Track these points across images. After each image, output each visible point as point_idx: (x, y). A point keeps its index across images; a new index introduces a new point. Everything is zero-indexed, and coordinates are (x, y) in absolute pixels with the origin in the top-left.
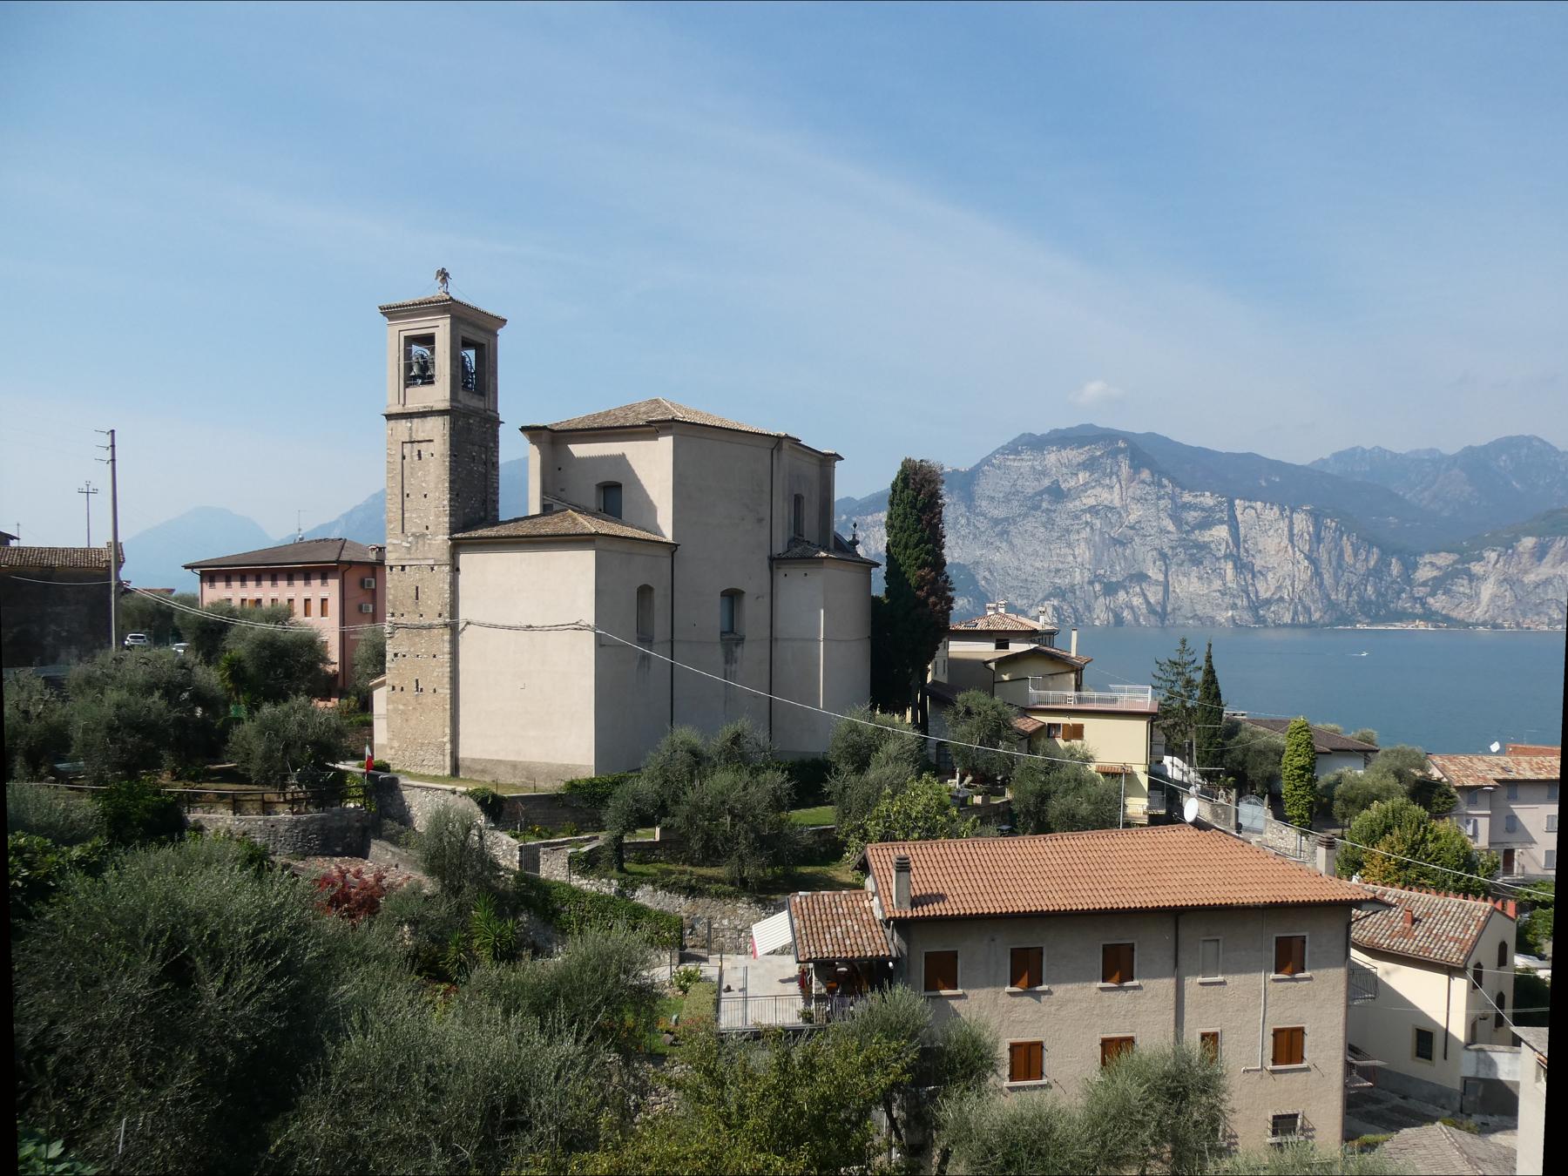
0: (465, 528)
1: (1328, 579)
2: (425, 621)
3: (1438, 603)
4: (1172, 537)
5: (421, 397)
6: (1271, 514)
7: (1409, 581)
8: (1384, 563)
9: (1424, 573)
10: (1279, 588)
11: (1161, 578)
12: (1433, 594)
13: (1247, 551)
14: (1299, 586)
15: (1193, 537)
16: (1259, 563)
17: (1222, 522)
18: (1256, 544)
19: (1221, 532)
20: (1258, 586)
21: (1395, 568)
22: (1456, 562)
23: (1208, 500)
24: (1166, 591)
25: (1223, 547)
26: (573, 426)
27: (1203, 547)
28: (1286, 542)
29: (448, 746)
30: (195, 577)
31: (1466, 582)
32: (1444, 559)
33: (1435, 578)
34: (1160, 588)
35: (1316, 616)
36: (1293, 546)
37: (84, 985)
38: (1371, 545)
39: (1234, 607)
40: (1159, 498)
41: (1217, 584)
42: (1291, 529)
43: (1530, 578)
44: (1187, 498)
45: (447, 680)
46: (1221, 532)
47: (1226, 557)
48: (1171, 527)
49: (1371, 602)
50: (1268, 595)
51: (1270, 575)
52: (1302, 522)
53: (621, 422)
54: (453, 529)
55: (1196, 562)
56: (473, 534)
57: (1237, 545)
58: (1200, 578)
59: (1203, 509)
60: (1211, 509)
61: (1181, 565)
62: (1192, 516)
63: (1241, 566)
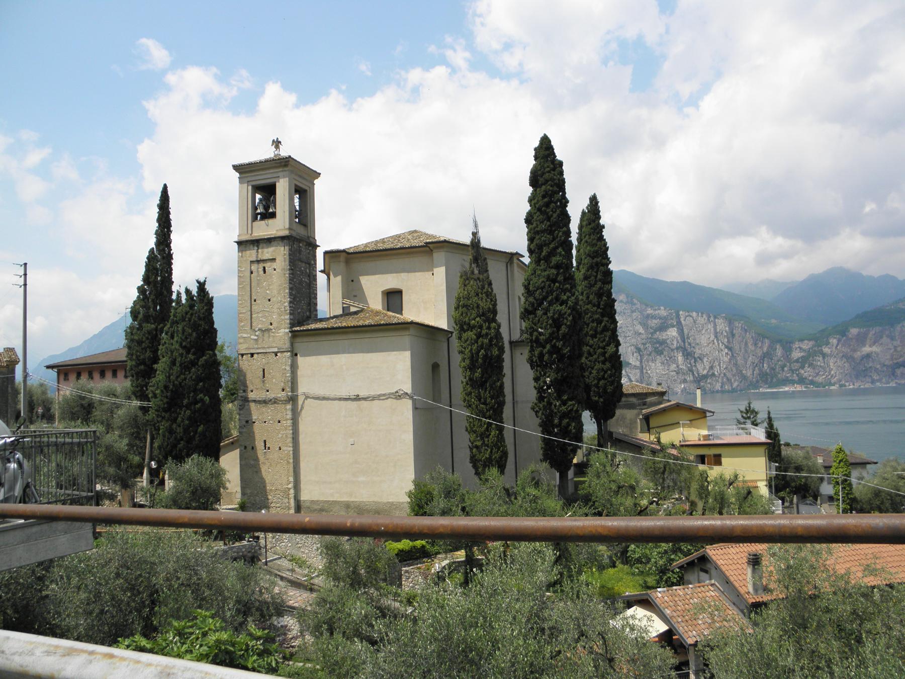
0: (300, 324)
1: (740, 361)
2: (270, 395)
3: (807, 372)
4: (644, 336)
5: (264, 229)
6: (702, 320)
7: (787, 358)
8: (772, 347)
9: (796, 355)
10: (711, 368)
11: (638, 364)
12: (803, 367)
13: (690, 344)
14: (723, 366)
15: (655, 336)
16: (698, 352)
17: (673, 326)
18: (694, 339)
19: (673, 332)
20: (698, 367)
21: (779, 351)
22: (814, 346)
23: (663, 312)
24: (642, 372)
25: (675, 343)
26: (361, 249)
27: (663, 342)
28: (712, 337)
29: (292, 491)
30: (53, 374)
31: (821, 359)
32: (807, 345)
33: (802, 357)
34: (638, 371)
35: (735, 385)
36: (718, 340)
37: (644, 666)
38: (764, 337)
39: (685, 381)
40: (633, 312)
41: (673, 367)
42: (715, 329)
43: (858, 355)
44: (649, 311)
45: (290, 440)
46: (673, 332)
47: (677, 348)
48: (641, 330)
49: (767, 374)
50: (705, 372)
51: (705, 360)
52: (722, 325)
53: (392, 246)
54: (292, 325)
55: (660, 353)
56: (309, 327)
57: (684, 342)
58: (663, 363)
59: (660, 318)
60: (665, 318)
61: (650, 355)
62: (654, 323)
63: (688, 355)
